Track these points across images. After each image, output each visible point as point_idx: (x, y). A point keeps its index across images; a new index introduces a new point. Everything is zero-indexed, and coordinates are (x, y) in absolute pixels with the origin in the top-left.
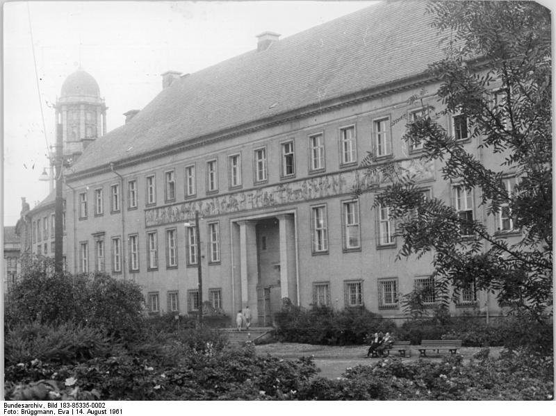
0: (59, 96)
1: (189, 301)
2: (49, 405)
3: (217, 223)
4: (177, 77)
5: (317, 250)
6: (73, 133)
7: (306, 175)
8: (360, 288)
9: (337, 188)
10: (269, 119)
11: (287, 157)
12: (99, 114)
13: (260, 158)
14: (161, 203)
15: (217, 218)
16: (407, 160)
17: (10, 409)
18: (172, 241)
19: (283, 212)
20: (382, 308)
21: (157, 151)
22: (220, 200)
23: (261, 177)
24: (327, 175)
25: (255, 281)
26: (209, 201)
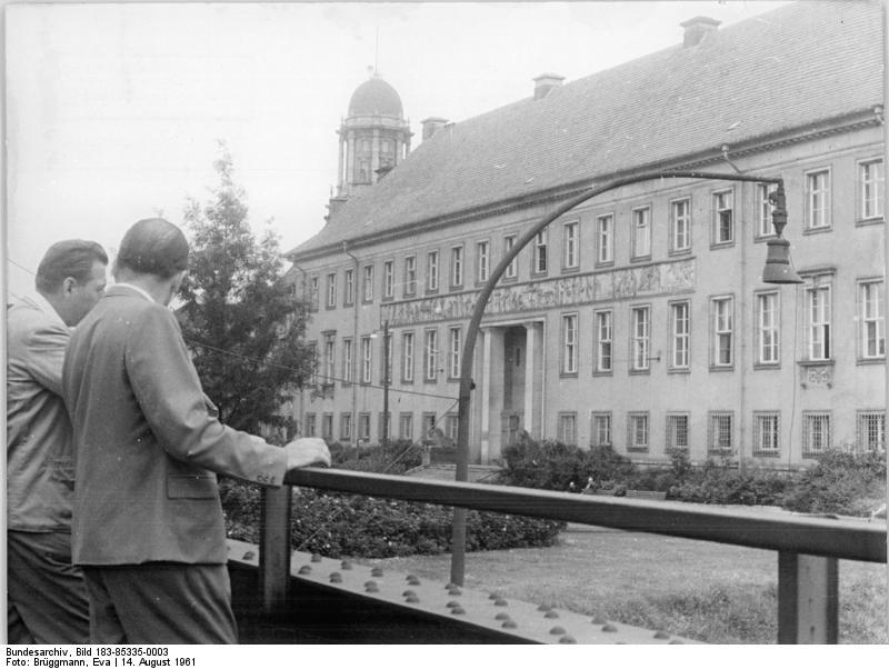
0: (346, 116)
1: (668, 432)
2: (78, 652)
3: (609, 312)
4: (443, 125)
5: (637, 368)
6: (362, 171)
7: (558, 274)
8: (776, 423)
9: (591, 293)
10: (520, 199)
11: (722, 214)
12: (399, 143)
13: (681, 213)
14: (444, 290)
15: (460, 322)
16: (666, 263)
17: (15, 658)
18: (410, 348)
19: (532, 320)
20: (757, 454)
21: (395, 230)
22: (465, 298)
23: (680, 245)
24: (581, 276)
25: (500, 405)
26: (453, 299)
